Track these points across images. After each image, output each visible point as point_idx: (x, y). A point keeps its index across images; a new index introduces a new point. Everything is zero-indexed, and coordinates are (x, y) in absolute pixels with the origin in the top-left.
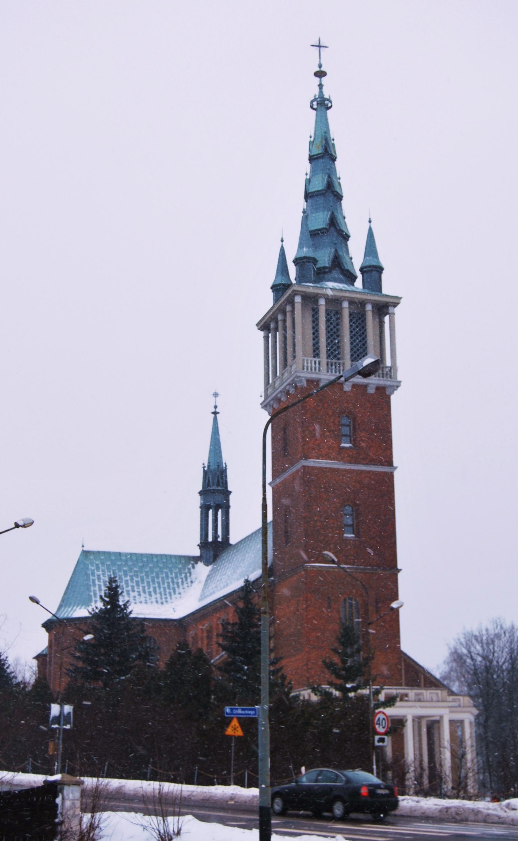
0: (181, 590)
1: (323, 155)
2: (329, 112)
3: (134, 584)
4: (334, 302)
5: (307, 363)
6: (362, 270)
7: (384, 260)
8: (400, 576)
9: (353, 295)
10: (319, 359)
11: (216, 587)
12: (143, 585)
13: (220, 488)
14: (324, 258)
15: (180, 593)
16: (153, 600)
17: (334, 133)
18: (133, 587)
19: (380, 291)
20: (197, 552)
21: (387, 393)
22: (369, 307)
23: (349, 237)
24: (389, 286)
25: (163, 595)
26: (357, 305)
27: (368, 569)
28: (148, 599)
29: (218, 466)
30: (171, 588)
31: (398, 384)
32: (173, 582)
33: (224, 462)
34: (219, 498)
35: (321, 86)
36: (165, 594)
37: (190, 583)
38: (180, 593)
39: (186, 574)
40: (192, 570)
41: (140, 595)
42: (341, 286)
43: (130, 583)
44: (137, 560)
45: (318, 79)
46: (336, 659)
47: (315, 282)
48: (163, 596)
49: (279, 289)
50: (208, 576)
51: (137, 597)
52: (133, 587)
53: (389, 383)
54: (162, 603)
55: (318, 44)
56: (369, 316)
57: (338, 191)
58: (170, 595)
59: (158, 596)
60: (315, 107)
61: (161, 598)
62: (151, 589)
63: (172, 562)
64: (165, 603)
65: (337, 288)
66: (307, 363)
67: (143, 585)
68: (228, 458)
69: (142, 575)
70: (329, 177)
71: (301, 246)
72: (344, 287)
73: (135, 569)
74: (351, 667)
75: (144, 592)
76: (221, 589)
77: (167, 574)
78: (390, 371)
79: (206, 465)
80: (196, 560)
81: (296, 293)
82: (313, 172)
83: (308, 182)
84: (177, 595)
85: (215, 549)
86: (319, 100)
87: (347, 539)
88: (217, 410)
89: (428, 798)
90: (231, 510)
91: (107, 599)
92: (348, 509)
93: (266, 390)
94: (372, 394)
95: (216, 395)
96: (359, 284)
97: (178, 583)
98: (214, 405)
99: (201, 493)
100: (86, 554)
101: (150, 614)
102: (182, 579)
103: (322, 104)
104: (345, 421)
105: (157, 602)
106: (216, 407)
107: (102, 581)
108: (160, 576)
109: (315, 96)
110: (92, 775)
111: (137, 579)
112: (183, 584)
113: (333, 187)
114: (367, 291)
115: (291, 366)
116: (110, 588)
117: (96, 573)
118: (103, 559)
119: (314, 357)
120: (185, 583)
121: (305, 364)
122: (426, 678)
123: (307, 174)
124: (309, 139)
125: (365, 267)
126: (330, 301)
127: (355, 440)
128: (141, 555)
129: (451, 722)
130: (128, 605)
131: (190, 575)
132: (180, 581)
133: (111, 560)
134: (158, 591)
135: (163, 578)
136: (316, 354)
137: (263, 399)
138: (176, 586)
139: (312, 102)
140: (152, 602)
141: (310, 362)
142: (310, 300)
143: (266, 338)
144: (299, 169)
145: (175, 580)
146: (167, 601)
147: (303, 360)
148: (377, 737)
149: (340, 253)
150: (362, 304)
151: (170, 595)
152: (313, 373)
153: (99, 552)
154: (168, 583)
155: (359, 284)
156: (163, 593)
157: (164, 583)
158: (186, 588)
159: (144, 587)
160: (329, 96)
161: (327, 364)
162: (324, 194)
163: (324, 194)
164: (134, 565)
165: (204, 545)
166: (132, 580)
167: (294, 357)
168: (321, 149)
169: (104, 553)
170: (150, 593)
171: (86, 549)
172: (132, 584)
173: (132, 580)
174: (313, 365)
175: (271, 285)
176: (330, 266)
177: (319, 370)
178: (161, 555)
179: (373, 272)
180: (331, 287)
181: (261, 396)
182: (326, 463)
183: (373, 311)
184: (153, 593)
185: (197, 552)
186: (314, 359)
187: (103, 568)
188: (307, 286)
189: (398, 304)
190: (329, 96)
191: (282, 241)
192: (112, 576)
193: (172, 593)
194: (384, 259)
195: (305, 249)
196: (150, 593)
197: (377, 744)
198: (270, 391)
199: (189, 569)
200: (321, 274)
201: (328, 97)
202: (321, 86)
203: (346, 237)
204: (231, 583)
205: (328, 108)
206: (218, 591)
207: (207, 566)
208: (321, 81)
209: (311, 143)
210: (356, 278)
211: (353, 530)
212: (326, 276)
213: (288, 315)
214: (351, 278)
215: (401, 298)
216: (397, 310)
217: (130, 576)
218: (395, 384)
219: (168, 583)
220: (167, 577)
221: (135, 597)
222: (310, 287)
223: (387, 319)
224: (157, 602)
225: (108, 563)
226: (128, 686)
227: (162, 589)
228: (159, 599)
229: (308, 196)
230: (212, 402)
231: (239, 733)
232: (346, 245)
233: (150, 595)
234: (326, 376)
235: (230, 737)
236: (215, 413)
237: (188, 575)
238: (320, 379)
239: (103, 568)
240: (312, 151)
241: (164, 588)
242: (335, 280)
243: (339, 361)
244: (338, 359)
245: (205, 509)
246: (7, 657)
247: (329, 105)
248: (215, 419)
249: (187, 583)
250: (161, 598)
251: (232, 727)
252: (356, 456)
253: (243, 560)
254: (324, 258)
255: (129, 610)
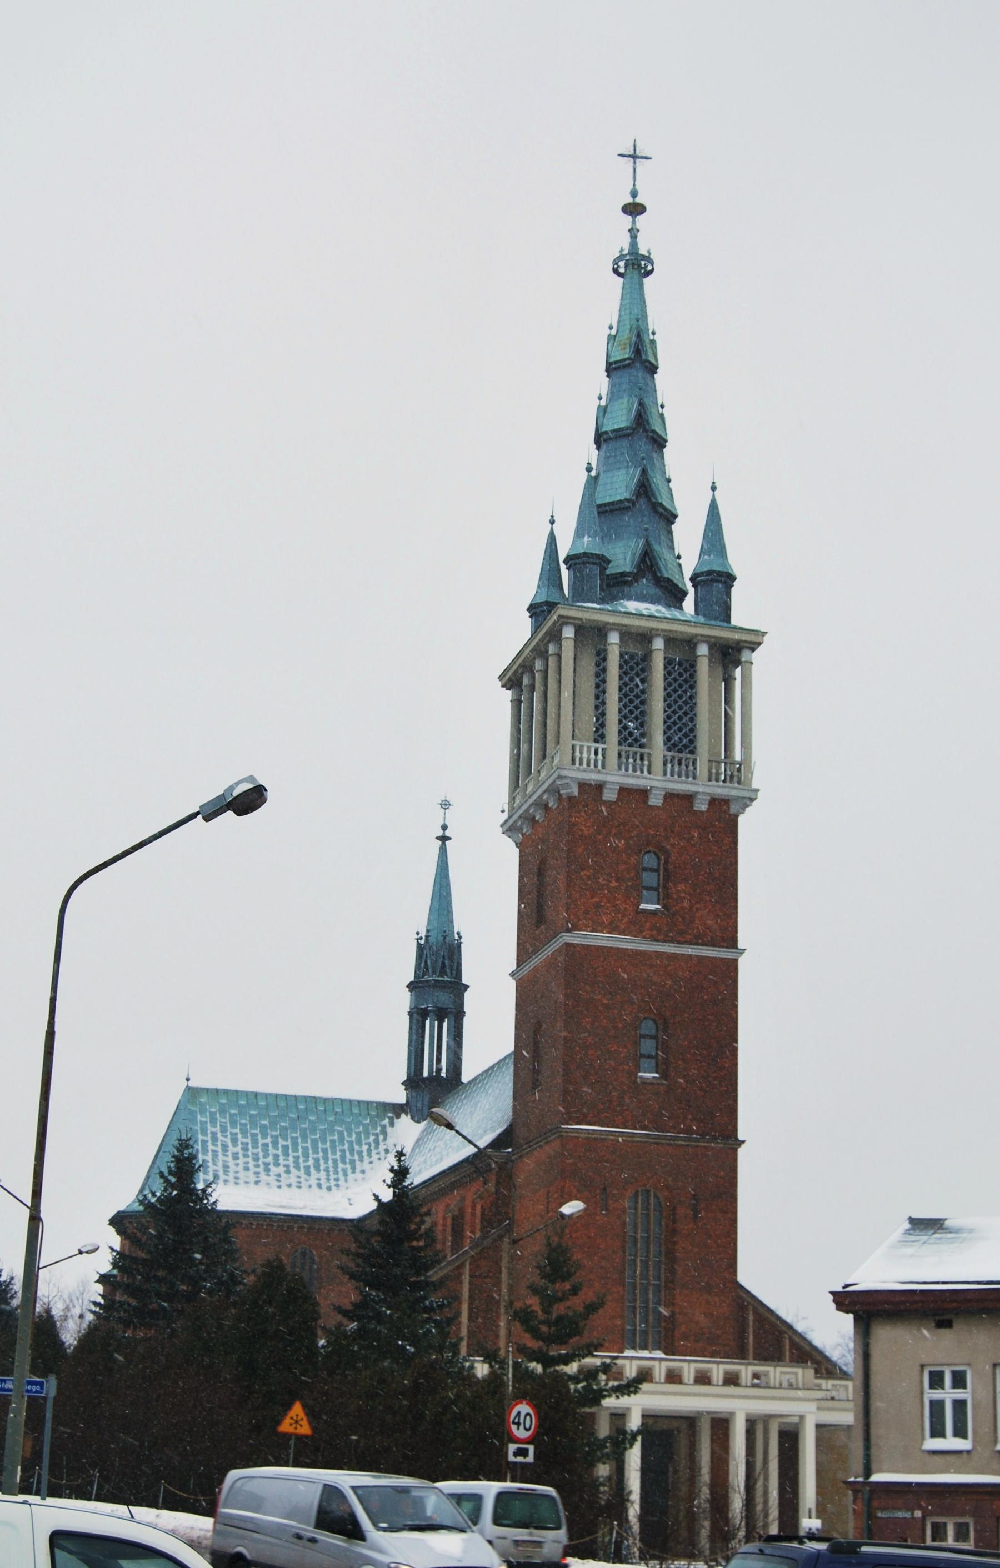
0: (366, 1166)
1: (633, 361)
2: (647, 281)
3: (280, 1152)
4: (639, 639)
5: (581, 753)
6: (692, 579)
7: (736, 561)
8: (741, 1151)
9: (675, 627)
10: (604, 746)
11: (425, 1162)
12: (296, 1154)
13: (446, 979)
14: (623, 556)
15: (363, 1172)
16: (313, 1182)
17: (657, 320)
18: (276, 1157)
19: (728, 618)
20: (400, 1096)
21: (732, 811)
22: (703, 650)
23: (676, 517)
24: (744, 612)
25: (331, 1173)
26: (683, 646)
27: (682, 1139)
28: (302, 1180)
29: (445, 937)
30: (347, 1161)
31: (753, 796)
32: (352, 1151)
33: (456, 931)
34: (444, 998)
35: (633, 233)
36: (337, 1173)
37: (383, 1153)
38: (363, 1172)
39: (377, 1135)
40: (389, 1129)
41: (288, 1172)
42: (653, 609)
43: (272, 1150)
44: (287, 1107)
45: (629, 218)
46: (534, 1302)
47: (602, 601)
48: (332, 1176)
49: (538, 611)
50: (418, 1140)
51: (283, 1175)
52: (276, 1157)
53: (734, 793)
54: (329, 1189)
55: (632, 153)
56: (703, 667)
57: (658, 429)
58: (345, 1175)
59: (323, 1175)
60: (622, 270)
61: (328, 1180)
62: (311, 1162)
63: (352, 1114)
64: (334, 1188)
65: (645, 612)
66: (581, 753)
67: (296, 1154)
68: (463, 922)
69: (294, 1135)
70: (641, 404)
71: (579, 534)
72: (657, 611)
73: (283, 1124)
74: (560, 1319)
75: (297, 1167)
76: (431, 1166)
77: (341, 1133)
78: (739, 770)
79: (423, 934)
80: (398, 1110)
81: (565, 620)
82: (613, 394)
83: (603, 411)
84: (358, 1175)
85: (432, 1090)
86: (628, 257)
87: (645, 1082)
88: (447, 833)
89: (585, 1561)
90: (467, 1022)
91: (173, 1180)
92: (648, 1027)
93: (512, 799)
94: (702, 812)
95: (445, 805)
96: (689, 604)
97: (360, 1153)
98: (442, 823)
99: (411, 986)
100: (192, 1094)
101: (304, 1207)
102: (369, 1144)
103: (635, 267)
104: (649, 860)
105: (319, 1186)
106: (444, 828)
107: (219, 1143)
108: (329, 1138)
109: (622, 250)
110: (905, 1518)
111: (285, 1143)
112: (369, 1155)
113: (648, 422)
114: (701, 619)
115: (553, 758)
116: (178, 1160)
117: (210, 1129)
118: (223, 1104)
119: (596, 741)
120: (374, 1152)
121: (577, 754)
122: (794, 1345)
123: (600, 398)
124: (608, 332)
125: (702, 574)
126: (627, 635)
127: (667, 896)
128: (296, 1098)
129: (819, 1427)
130: (210, 1190)
131: (385, 1139)
132: (365, 1148)
133: (240, 1106)
134: (322, 1166)
135: (333, 1141)
136: (600, 737)
137: (506, 815)
138: (356, 1157)
139: (616, 262)
140: (310, 1186)
141: (587, 748)
142: (591, 635)
143: (517, 703)
144: (586, 388)
145: (357, 1148)
146: (337, 1186)
147: (573, 747)
148: (512, 1447)
149: (656, 547)
150: (690, 643)
151: (345, 1175)
152: (591, 771)
153: (217, 1090)
154: (343, 1151)
155: (689, 604)
156: (331, 1169)
157: (334, 1153)
158: (376, 1162)
159: (297, 1158)
160: (649, 252)
161: (620, 755)
162: (633, 435)
163: (633, 435)
164: (282, 1116)
165: (413, 1082)
166: (275, 1144)
167: (558, 743)
168: (628, 350)
169: (226, 1092)
170: (307, 1170)
171: (192, 1084)
172: (275, 1152)
173: (275, 1144)
174: (593, 756)
175: (527, 605)
176: (635, 571)
177: (603, 766)
178: (333, 1100)
179: (716, 583)
180: (638, 608)
181: (503, 812)
182: (608, 939)
183: (711, 656)
184: (312, 1169)
185: (400, 1096)
186: (594, 745)
187: (223, 1120)
188: (588, 608)
189: (760, 644)
190: (649, 252)
191: (552, 522)
192: (184, 1137)
193: (349, 1171)
194: (737, 559)
195: (586, 539)
196: (307, 1170)
197: (511, 1458)
198: (518, 801)
199: (384, 1127)
200: (616, 585)
201: (646, 254)
202: (633, 233)
203: (669, 517)
204: (447, 1154)
205: (649, 273)
206: (427, 1169)
207: (418, 1122)
208: (634, 222)
209: (611, 339)
210: (685, 594)
211: (657, 1064)
212: (626, 589)
213: (552, 662)
214: (674, 595)
215: (764, 633)
216: (758, 658)
217: (272, 1136)
218: (746, 794)
219: (343, 1151)
220: (342, 1140)
221: (279, 1175)
222: (592, 611)
223: (738, 672)
224: (319, 1186)
225: (233, 1111)
226: (213, 1339)
227: (330, 1162)
228: (323, 1181)
229: (601, 439)
230: (438, 816)
231: (305, 1429)
232: (670, 533)
233: (308, 1173)
234: (615, 778)
235: (287, 1436)
236: (444, 839)
237: (381, 1137)
238: (605, 782)
239: (223, 1120)
240: (612, 354)
241: (335, 1161)
242: (641, 598)
243: (643, 750)
244: (642, 746)
245: (418, 1016)
246: (12, 1278)
247: (649, 268)
248: (443, 851)
249: (378, 1153)
250: (328, 1180)
251: (292, 1418)
252: (671, 925)
253: (472, 1113)
254: (623, 556)
255: (212, 1200)
